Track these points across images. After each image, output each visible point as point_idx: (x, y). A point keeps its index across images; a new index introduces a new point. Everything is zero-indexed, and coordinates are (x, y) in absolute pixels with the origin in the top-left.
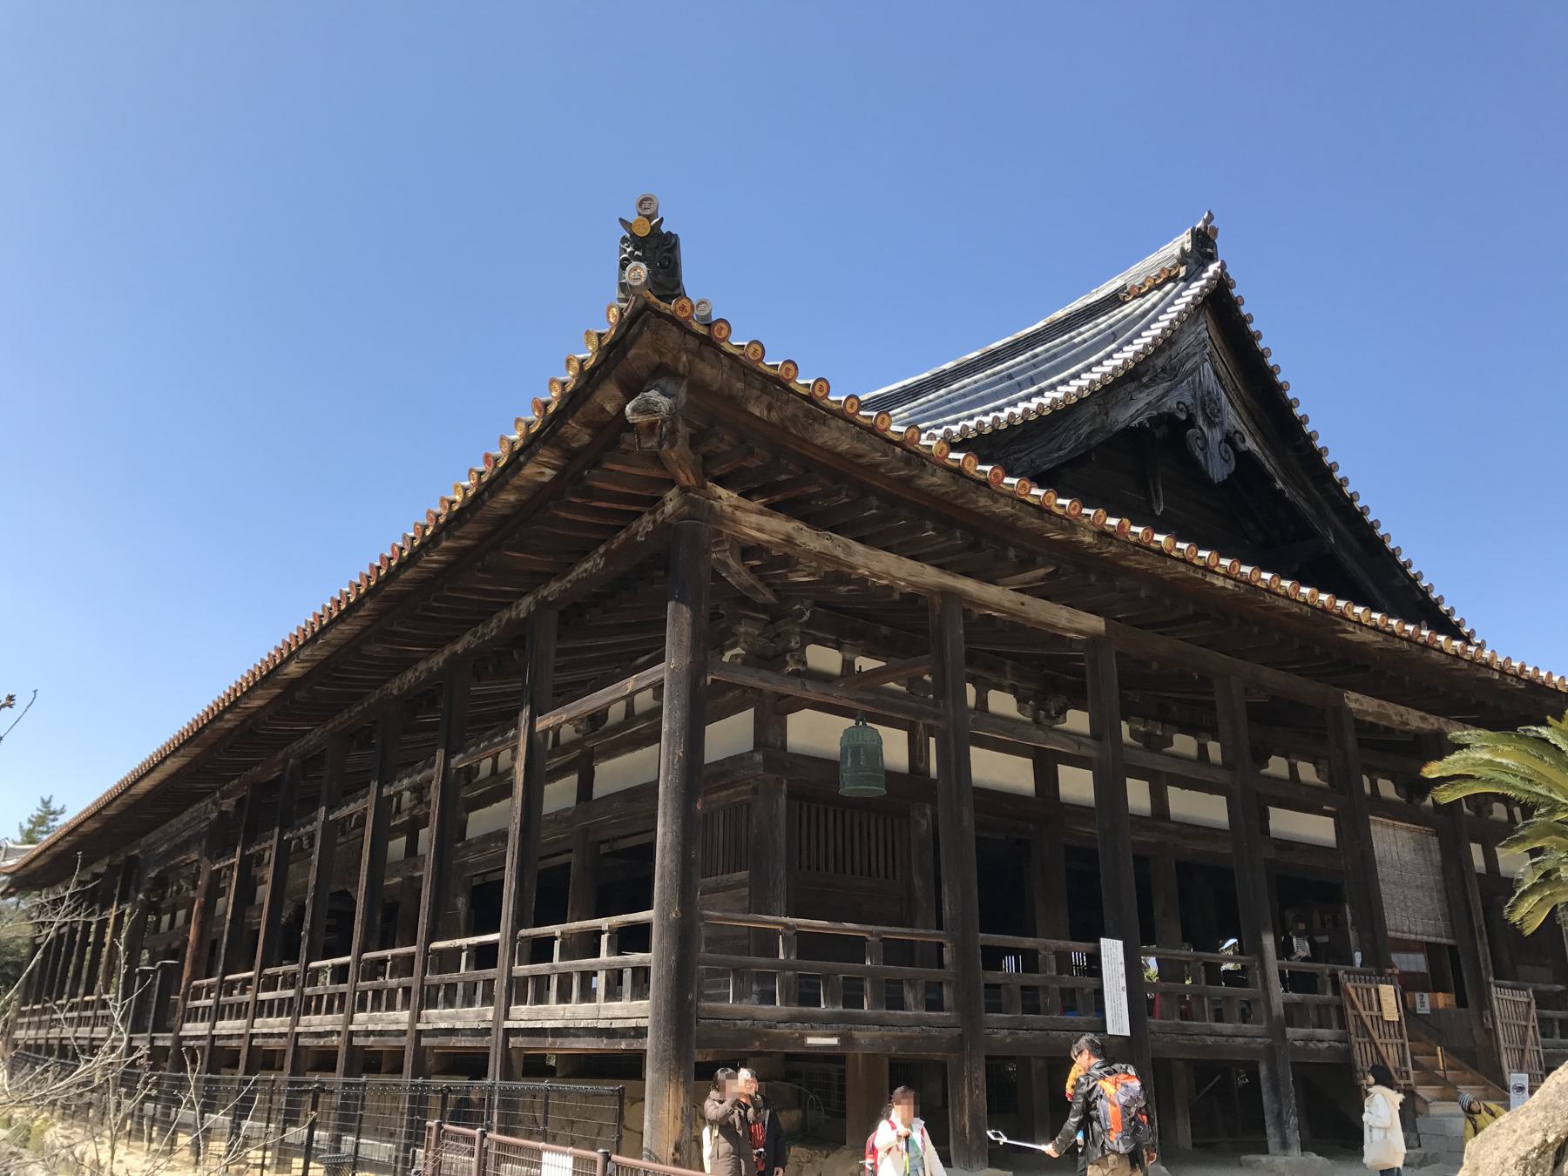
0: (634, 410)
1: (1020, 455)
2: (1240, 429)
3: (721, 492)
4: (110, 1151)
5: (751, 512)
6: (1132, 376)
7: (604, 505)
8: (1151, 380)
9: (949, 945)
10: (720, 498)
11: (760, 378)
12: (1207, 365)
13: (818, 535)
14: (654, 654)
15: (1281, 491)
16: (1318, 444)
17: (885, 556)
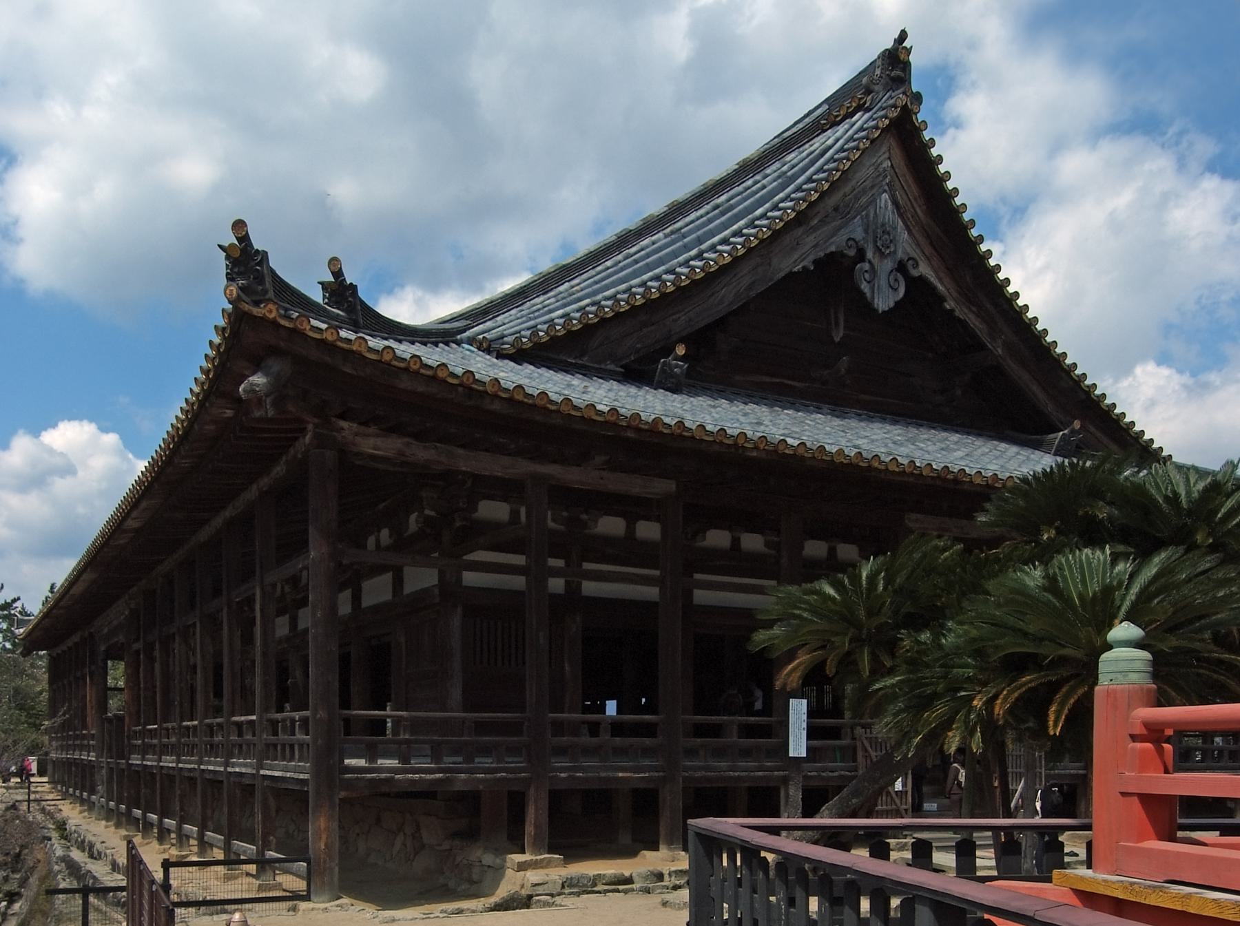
0: (244, 390)
4: (411, 917)
10: (343, 429)
12: (885, 196)
15: (952, 311)
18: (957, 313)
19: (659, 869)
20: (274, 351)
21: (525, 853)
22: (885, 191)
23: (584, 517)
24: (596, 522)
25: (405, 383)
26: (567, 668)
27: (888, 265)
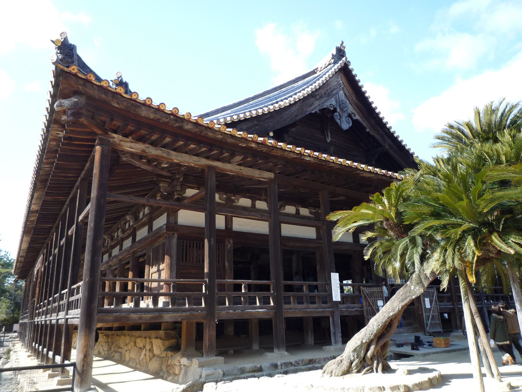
0: (56, 106)
1: (269, 123)
2: (354, 112)
3: (114, 135)
5: (128, 142)
6: (313, 95)
7: (77, 143)
8: (320, 97)
9: (273, 281)
10: (114, 137)
11: (111, 93)
13: (156, 149)
14: (148, 195)
15: (369, 132)
16: (381, 116)
17: (184, 155)
18: (371, 133)
19: (275, 362)
20: (76, 93)
21: (203, 356)
22: (341, 90)
23: (233, 198)
24: (238, 200)
25: (144, 112)
26: (227, 264)
27: (346, 115)
